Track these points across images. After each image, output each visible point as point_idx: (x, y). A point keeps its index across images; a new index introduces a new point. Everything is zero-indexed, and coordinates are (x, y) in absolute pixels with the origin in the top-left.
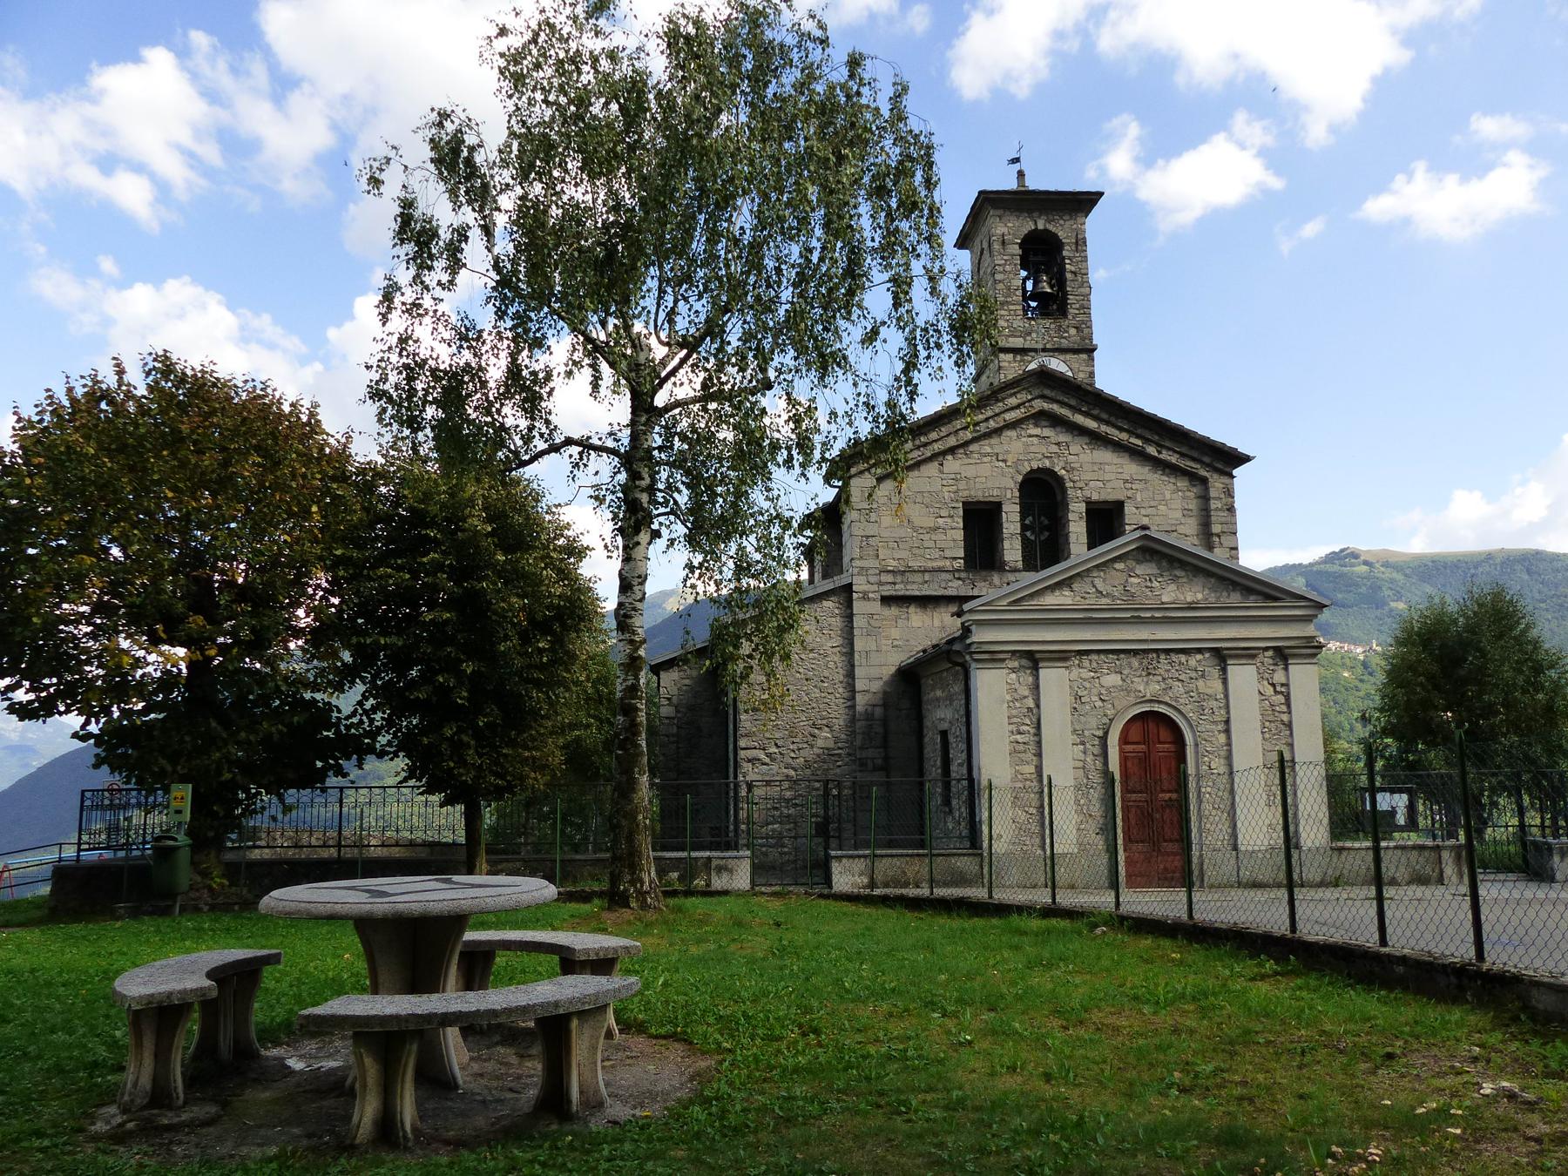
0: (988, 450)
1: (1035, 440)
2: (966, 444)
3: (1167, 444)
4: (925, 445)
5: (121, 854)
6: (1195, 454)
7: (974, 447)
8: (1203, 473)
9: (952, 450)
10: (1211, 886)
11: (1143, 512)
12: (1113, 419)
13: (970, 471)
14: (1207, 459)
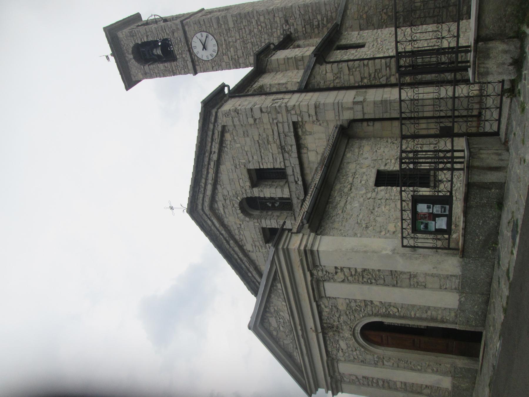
0: (237, 231)
1: (226, 210)
2: (236, 242)
3: (208, 148)
4: (241, 260)
5: (411, 166)
6: (210, 133)
7: (237, 237)
8: (220, 129)
9: (241, 248)
10: (484, 325)
11: (251, 159)
12: (204, 176)
13: (250, 240)
14: (211, 126)
